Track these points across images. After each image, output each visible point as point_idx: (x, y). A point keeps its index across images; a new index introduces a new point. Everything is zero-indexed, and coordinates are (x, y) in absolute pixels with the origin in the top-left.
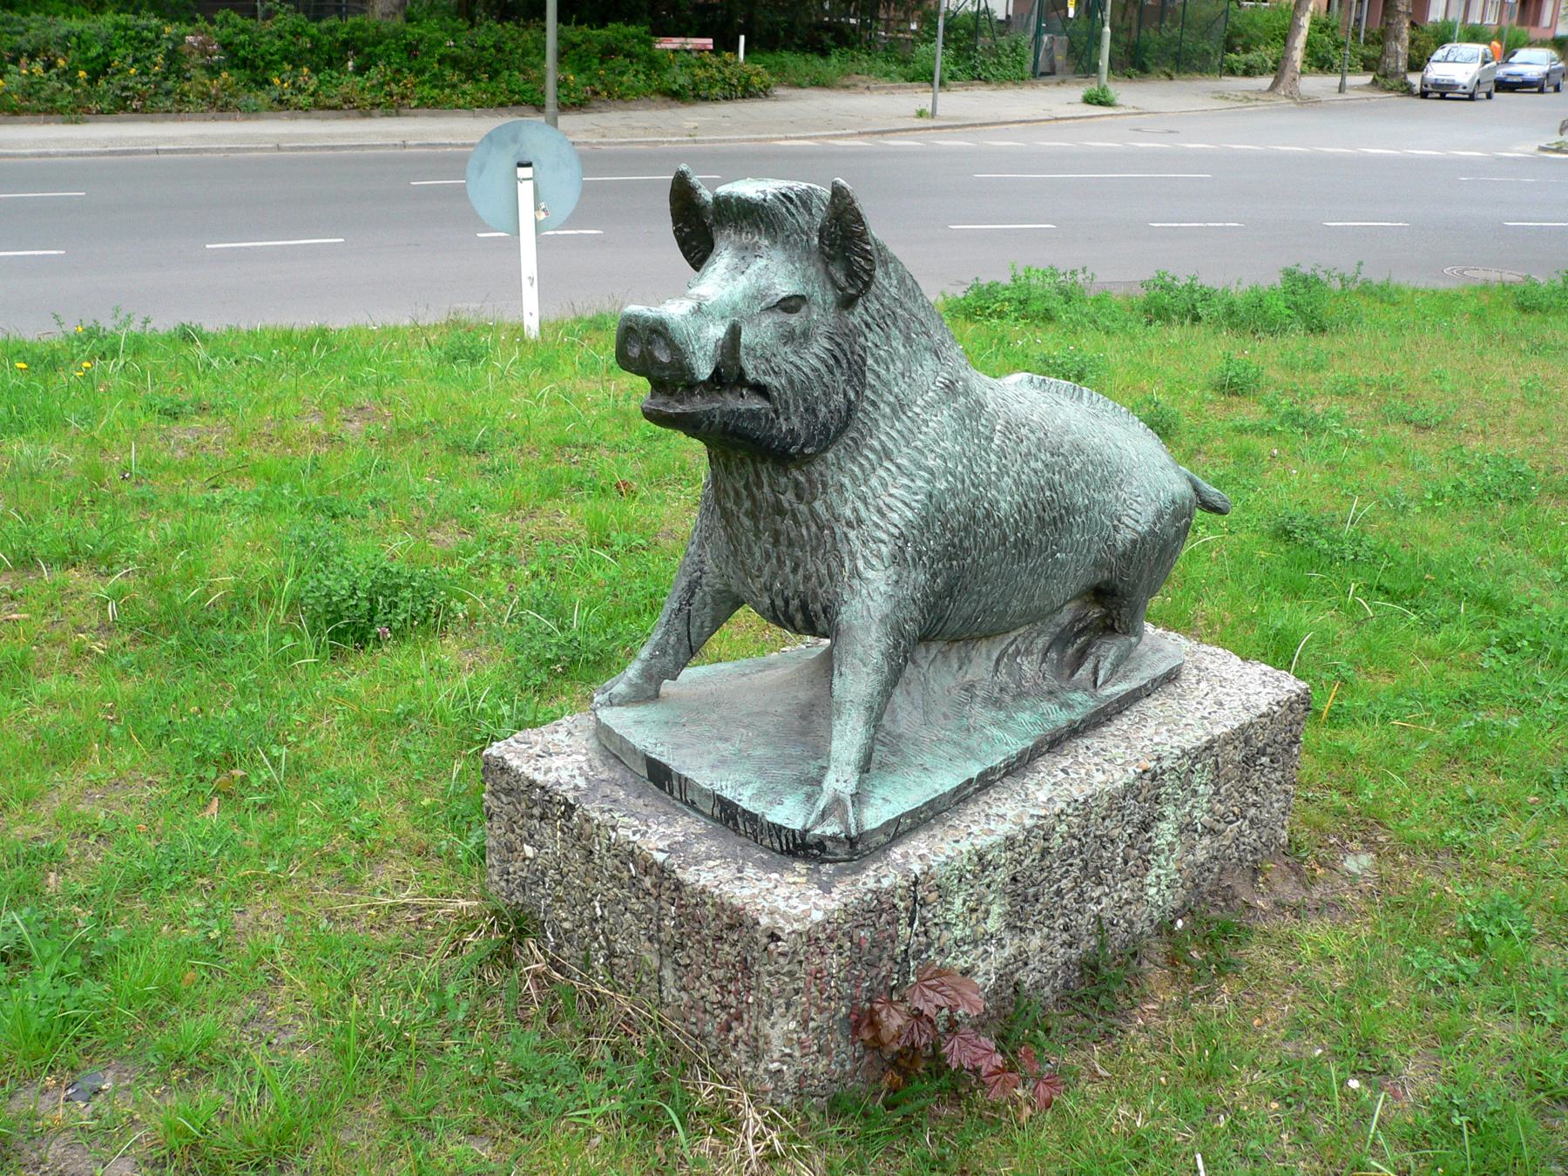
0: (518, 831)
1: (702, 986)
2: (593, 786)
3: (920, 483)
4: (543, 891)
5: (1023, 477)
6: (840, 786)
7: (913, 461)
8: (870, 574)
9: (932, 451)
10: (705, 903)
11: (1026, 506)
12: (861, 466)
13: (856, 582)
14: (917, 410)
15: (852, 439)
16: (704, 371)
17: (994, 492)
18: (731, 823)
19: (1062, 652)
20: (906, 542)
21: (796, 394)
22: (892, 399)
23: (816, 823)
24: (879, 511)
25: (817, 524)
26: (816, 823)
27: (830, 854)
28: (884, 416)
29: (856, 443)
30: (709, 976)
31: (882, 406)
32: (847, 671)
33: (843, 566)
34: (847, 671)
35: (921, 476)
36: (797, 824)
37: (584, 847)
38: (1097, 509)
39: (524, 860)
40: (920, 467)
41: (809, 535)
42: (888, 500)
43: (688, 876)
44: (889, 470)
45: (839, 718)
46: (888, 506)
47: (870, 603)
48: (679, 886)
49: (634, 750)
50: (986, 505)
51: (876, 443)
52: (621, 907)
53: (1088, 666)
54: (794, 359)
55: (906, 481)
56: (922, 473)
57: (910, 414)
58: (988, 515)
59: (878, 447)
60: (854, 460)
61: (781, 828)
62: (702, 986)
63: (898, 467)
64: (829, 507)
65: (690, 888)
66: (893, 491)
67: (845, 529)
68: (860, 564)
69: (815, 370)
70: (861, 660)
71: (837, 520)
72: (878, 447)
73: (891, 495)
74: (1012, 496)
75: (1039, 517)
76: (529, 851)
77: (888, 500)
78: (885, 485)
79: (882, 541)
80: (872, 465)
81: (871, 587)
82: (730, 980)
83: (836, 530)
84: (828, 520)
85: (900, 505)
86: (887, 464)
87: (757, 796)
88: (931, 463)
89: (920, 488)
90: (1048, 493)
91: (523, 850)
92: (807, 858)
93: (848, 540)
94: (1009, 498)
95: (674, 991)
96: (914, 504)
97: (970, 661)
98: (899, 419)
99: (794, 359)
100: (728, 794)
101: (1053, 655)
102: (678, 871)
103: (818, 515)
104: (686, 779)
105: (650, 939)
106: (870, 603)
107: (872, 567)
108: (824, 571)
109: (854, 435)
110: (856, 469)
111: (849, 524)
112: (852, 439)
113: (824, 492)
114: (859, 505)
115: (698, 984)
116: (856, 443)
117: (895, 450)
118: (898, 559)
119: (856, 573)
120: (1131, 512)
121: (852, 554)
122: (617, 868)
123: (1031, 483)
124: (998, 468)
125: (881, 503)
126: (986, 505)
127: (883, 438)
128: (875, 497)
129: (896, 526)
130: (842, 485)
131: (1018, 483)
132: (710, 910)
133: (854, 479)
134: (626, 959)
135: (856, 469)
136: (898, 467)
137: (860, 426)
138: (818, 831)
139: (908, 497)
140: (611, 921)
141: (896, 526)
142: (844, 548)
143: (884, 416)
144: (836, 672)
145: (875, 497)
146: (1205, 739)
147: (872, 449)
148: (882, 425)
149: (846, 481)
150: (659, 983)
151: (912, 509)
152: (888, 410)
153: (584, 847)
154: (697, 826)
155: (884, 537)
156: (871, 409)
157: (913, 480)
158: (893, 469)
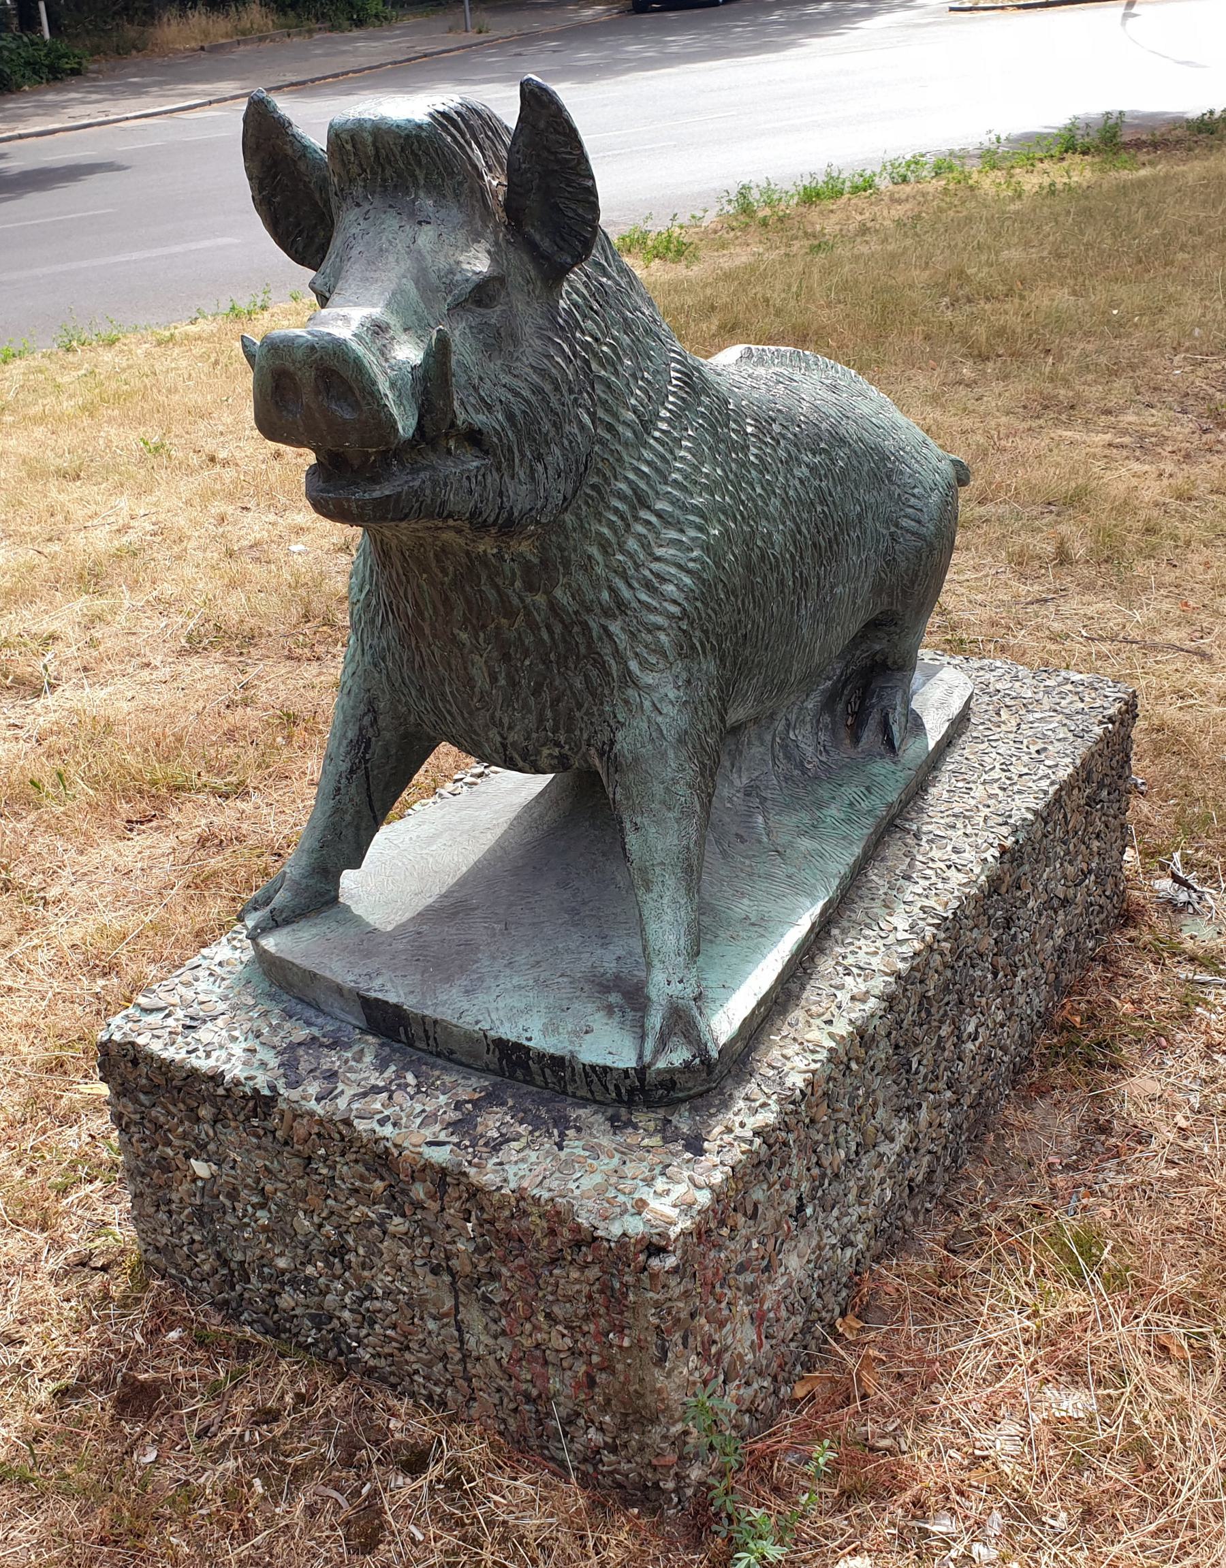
0: (176, 1142)
1: (536, 1328)
2: (290, 1058)
3: (693, 533)
4: (234, 1221)
5: (791, 493)
6: (675, 989)
7: (674, 502)
8: (648, 679)
9: (696, 482)
10: (525, 1213)
11: (800, 532)
12: (611, 524)
13: (631, 693)
14: (664, 426)
15: (593, 487)
16: (405, 424)
17: (764, 523)
18: (519, 1074)
19: (832, 712)
20: (691, 624)
21: (518, 432)
22: (630, 416)
23: (657, 1053)
24: (649, 587)
25: (562, 621)
26: (657, 1053)
27: (681, 1090)
28: (626, 444)
29: (599, 492)
30: (548, 1316)
31: (620, 429)
32: (646, 821)
33: (609, 674)
34: (646, 821)
35: (691, 522)
36: (626, 1059)
37: (298, 1155)
38: (870, 515)
39: (194, 1181)
40: (683, 508)
41: (552, 638)
42: (656, 566)
43: (488, 1177)
44: (648, 522)
45: (649, 890)
46: (657, 575)
47: (660, 719)
48: (475, 1192)
49: (339, 990)
50: (759, 543)
51: (623, 486)
52: (376, 1230)
53: (874, 720)
54: (505, 379)
55: (673, 534)
56: (692, 518)
57: (657, 434)
58: (763, 557)
59: (629, 492)
60: (599, 516)
61: (606, 1070)
62: (536, 1328)
63: (659, 514)
64: (576, 594)
65: (497, 1196)
66: (660, 552)
67: (603, 621)
68: (633, 665)
69: (537, 390)
70: (664, 802)
71: (589, 610)
72: (629, 492)
73: (658, 559)
74: (784, 523)
75: (814, 544)
76: (201, 1168)
77: (656, 566)
78: (646, 547)
79: (660, 628)
80: (622, 518)
81: (656, 696)
82: (586, 1318)
83: (592, 624)
84: (576, 613)
85: (673, 570)
86: (645, 514)
87: (551, 1028)
88: (697, 501)
89: (693, 539)
90: (819, 509)
91: (190, 1167)
92: (651, 1105)
93: (609, 635)
94: (781, 527)
95: (485, 1338)
96: (691, 565)
97: (741, 753)
98: (646, 445)
99: (505, 379)
100: (509, 1032)
101: (827, 719)
102: (472, 1171)
103: (563, 608)
104: (436, 1022)
105: (435, 1271)
106: (660, 719)
107: (651, 668)
108: (579, 684)
109: (595, 480)
110: (605, 530)
111: (607, 613)
112: (593, 487)
113: (567, 573)
114: (620, 584)
115: (528, 1326)
116: (599, 492)
117: (650, 492)
118: (687, 650)
119: (628, 678)
120: (910, 510)
121: (617, 653)
122: (362, 1178)
123: (800, 500)
124: (763, 488)
125: (647, 573)
126: (759, 543)
127: (631, 476)
128: (637, 566)
129: (675, 602)
130: (590, 557)
131: (786, 502)
132: (535, 1221)
133: (605, 547)
134: (395, 1302)
135: (605, 530)
136: (659, 514)
137: (600, 465)
138: (661, 1064)
139: (681, 557)
140: (361, 1251)
141: (675, 602)
142: (607, 650)
143: (626, 444)
144: (628, 825)
145: (637, 566)
146: (1052, 790)
147: (621, 496)
148: (626, 458)
149: (594, 551)
150: (459, 1330)
151: (689, 572)
152: (629, 434)
153: (298, 1155)
154: (469, 1087)
155: (660, 620)
156: (608, 436)
157: (682, 531)
158: (654, 519)
